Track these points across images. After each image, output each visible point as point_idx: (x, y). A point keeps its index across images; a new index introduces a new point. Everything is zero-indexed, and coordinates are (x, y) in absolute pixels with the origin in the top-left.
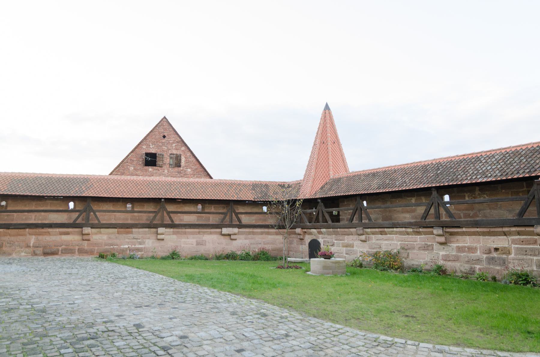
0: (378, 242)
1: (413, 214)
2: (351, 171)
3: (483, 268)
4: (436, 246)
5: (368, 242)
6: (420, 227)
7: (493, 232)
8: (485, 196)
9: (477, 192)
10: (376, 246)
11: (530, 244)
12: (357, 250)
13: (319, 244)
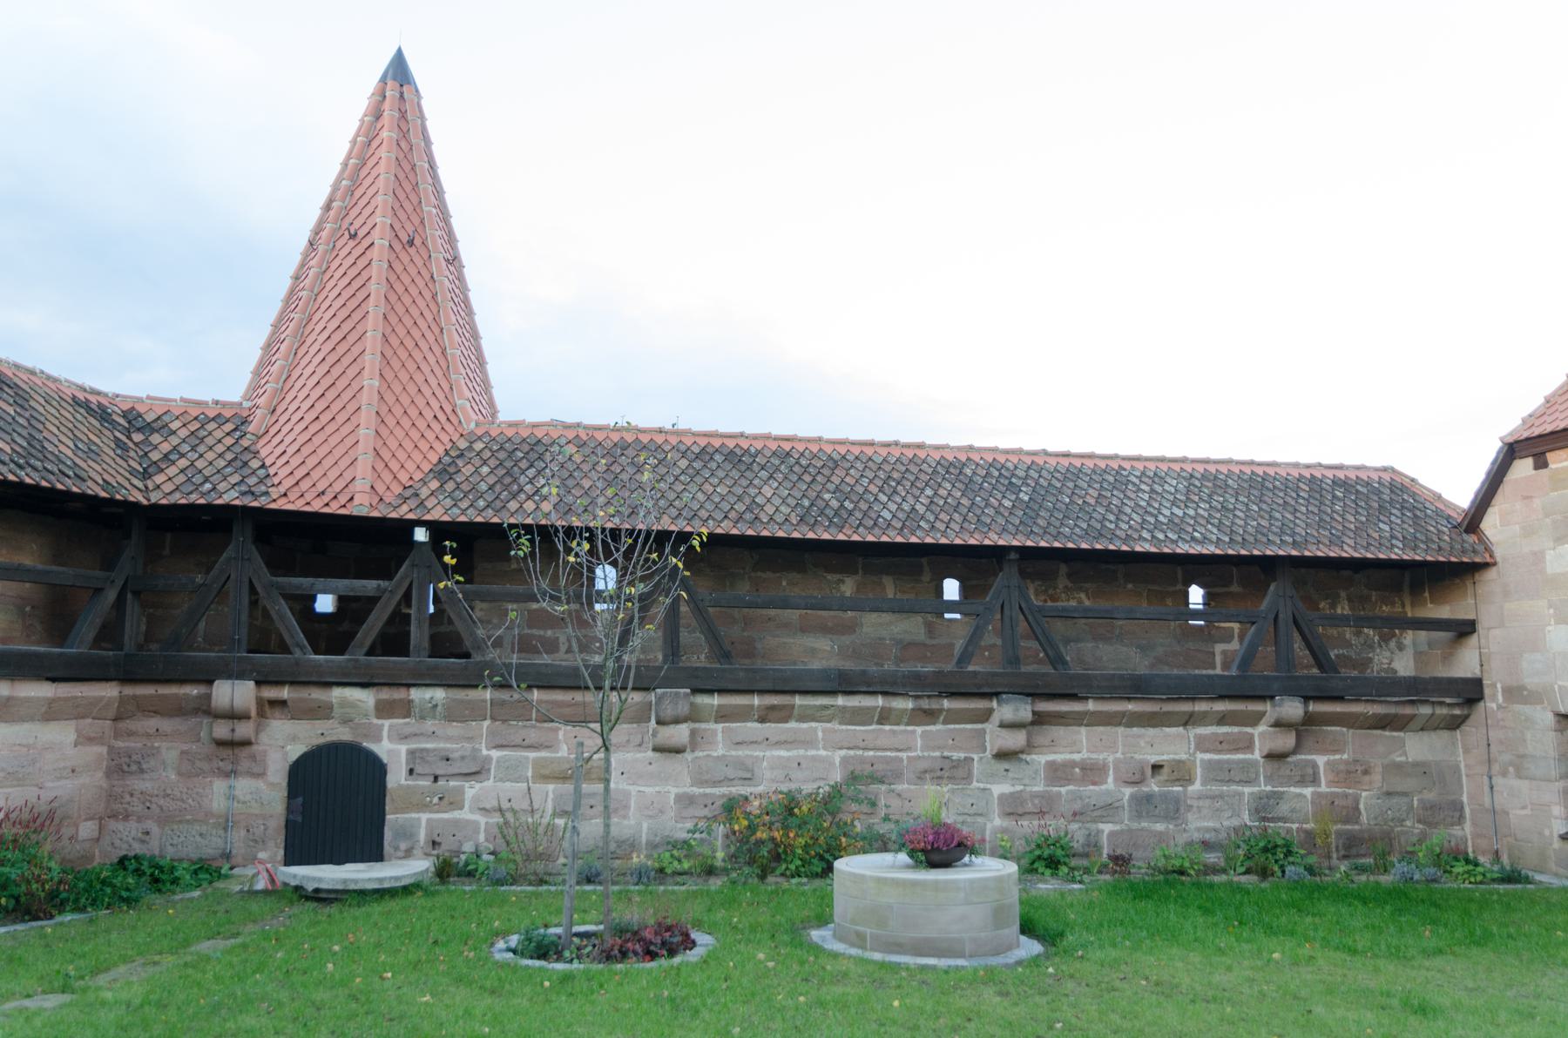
0: (741, 752)
1: (846, 639)
2: (503, 416)
3: (1121, 832)
4: (980, 763)
5: (688, 756)
6: (940, 695)
7: (1168, 713)
8: (1083, 596)
9: (1062, 582)
10: (731, 773)
11: (1237, 750)
12: (627, 794)
13: (377, 769)
